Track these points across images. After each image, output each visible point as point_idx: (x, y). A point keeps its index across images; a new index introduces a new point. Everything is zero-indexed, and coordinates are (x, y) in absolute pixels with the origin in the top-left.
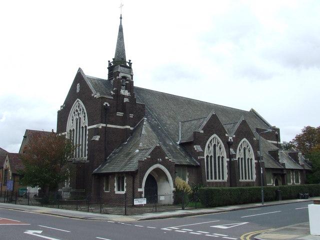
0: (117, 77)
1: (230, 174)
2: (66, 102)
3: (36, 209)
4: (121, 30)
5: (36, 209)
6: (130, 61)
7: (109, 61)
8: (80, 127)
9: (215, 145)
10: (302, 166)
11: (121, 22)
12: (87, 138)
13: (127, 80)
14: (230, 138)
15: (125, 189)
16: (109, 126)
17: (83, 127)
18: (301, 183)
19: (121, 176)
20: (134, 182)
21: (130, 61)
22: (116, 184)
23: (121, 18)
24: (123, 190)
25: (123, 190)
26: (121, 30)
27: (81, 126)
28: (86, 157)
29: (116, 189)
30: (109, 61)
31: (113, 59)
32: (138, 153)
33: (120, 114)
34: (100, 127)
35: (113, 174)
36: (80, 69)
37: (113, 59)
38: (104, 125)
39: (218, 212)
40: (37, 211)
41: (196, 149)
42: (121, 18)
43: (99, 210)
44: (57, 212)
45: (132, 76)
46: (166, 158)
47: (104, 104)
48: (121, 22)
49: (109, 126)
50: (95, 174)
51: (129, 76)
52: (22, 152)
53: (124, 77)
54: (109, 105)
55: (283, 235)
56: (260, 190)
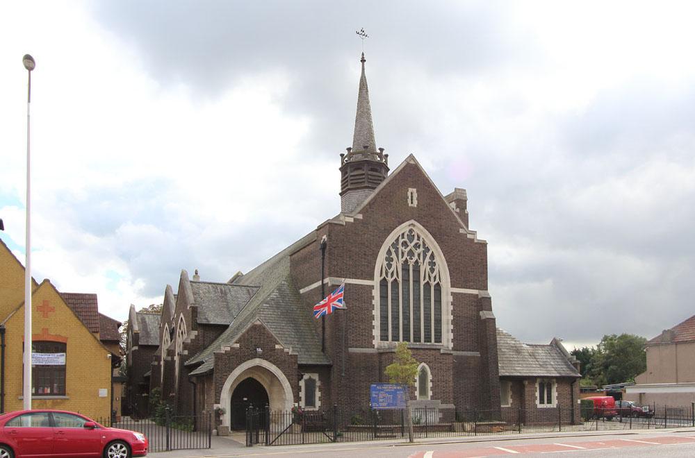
4: (29, 101)
6: (381, 150)
7: (342, 155)
11: (363, 69)
12: (498, 422)
16: (475, 292)
21: (381, 150)
22: (537, 394)
23: (363, 61)
24: (549, 401)
26: (29, 101)
27: (422, 283)
30: (342, 155)
31: (349, 149)
35: (532, 379)
36: (411, 157)
37: (349, 149)
39: (195, 403)
42: (363, 61)
46: (277, 347)
48: (363, 69)
49: (475, 292)
56: (371, 277)
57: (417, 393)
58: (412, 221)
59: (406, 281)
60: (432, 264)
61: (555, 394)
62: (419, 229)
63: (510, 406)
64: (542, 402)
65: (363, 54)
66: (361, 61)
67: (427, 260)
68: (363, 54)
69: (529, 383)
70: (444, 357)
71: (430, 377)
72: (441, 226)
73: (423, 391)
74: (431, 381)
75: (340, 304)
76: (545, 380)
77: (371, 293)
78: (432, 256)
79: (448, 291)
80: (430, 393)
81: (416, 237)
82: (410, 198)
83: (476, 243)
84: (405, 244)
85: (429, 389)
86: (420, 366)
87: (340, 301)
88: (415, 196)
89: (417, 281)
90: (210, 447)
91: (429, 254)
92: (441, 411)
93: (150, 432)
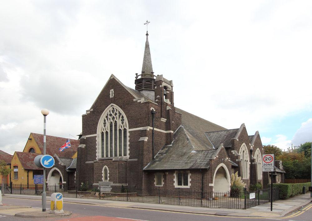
0: (161, 86)
1: (251, 173)
2: (94, 107)
3: (107, 203)
4: (147, 46)
5: (107, 203)
8: (116, 130)
9: (244, 151)
10: (282, 170)
11: (147, 38)
13: (168, 91)
14: (252, 147)
15: (189, 184)
16: (155, 129)
17: (120, 130)
18: (280, 183)
19: (182, 174)
20: (203, 178)
23: (147, 35)
24: (186, 184)
25: (186, 184)
26: (147, 46)
27: (118, 129)
28: (128, 156)
29: (155, 183)
32: (196, 154)
33: (164, 120)
34: (148, 130)
35: (172, 171)
38: (152, 128)
40: (110, 204)
41: (233, 153)
42: (147, 35)
43: (19, 192)
44: (138, 205)
45: (172, 87)
47: (151, 109)
48: (147, 38)
49: (155, 129)
50: (145, 171)
51: (169, 86)
52: (27, 151)
53: (165, 87)
54: (154, 110)
55: (160, 206)
57: (103, 179)
58: (112, 104)
59: (111, 130)
60: (123, 120)
61: (189, 180)
62: (116, 106)
63: (162, 186)
64: (180, 183)
65: (147, 32)
66: (146, 35)
67: (121, 119)
68: (147, 32)
69: (168, 173)
70: (115, 162)
71: (108, 172)
72: (124, 101)
73: (106, 178)
74: (102, 173)
75: (69, 146)
76: (182, 172)
77: (96, 139)
78: (123, 117)
79: (128, 130)
80: (108, 179)
81: (115, 110)
82: (113, 93)
83: (142, 103)
84: (111, 115)
85: (156, 181)
86: (104, 167)
87: (69, 145)
88: (113, 92)
89: (116, 130)
90: (159, 203)
91: (121, 116)
92: (112, 186)
93: (173, 200)
